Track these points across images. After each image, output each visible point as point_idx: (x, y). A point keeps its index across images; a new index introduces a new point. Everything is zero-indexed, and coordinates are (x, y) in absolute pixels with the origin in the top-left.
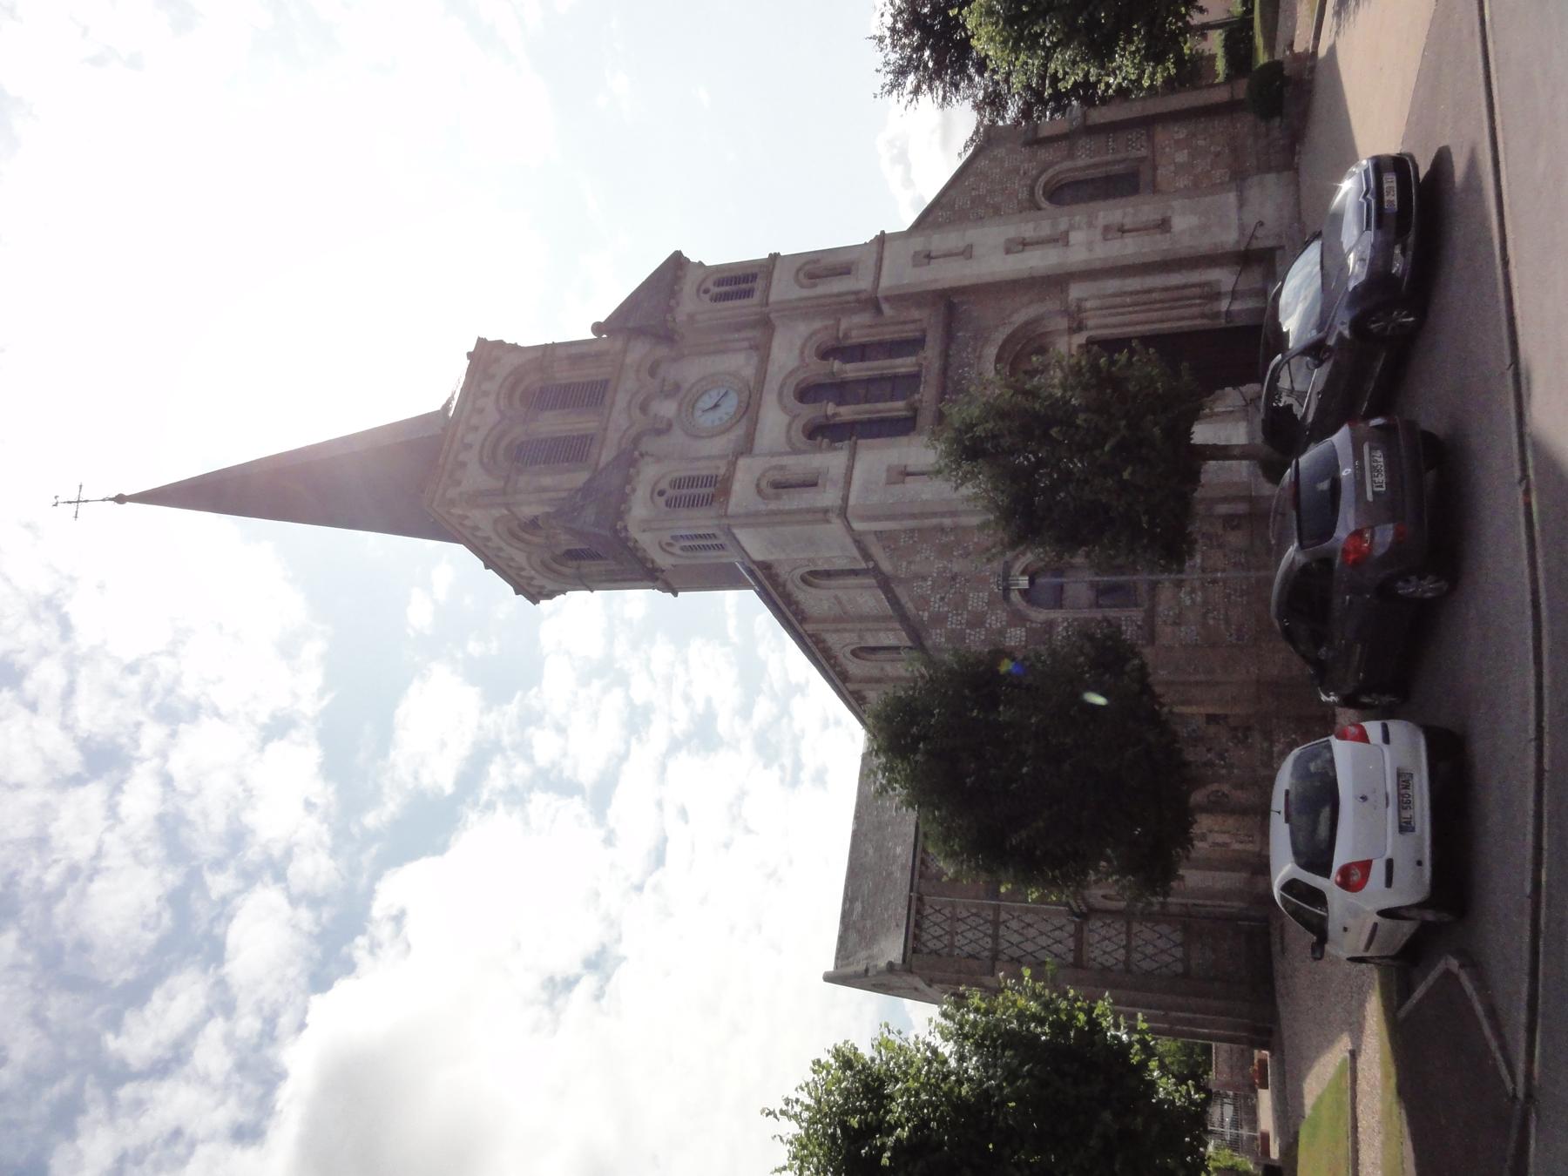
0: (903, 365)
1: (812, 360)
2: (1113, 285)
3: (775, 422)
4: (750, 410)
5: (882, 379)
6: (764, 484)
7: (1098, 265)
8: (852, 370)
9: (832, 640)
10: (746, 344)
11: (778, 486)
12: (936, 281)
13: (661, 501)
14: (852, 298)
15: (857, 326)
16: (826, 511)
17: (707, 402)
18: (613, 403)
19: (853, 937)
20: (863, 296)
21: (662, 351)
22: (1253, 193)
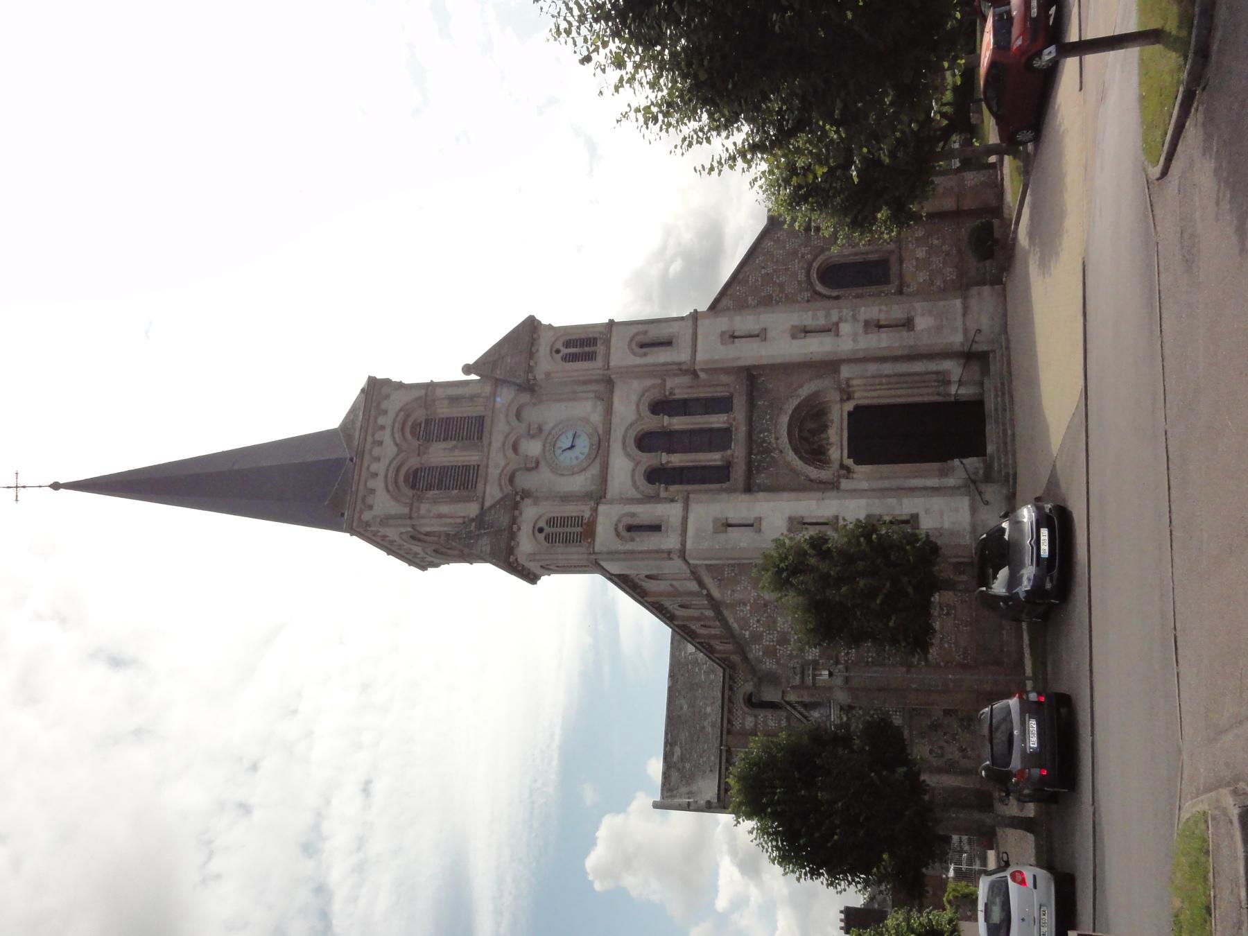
0: (717, 421)
1: (646, 413)
2: (872, 368)
3: (623, 469)
4: (601, 448)
5: (701, 432)
6: (620, 528)
7: (861, 355)
8: (678, 423)
9: (667, 603)
10: (592, 395)
11: (630, 528)
12: (739, 358)
13: (541, 536)
14: (674, 367)
15: (679, 388)
16: (669, 552)
17: (565, 442)
18: (490, 443)
19: (675, 775)
20: (684, 367)
21: (525, 398)
22: (973, 302)
